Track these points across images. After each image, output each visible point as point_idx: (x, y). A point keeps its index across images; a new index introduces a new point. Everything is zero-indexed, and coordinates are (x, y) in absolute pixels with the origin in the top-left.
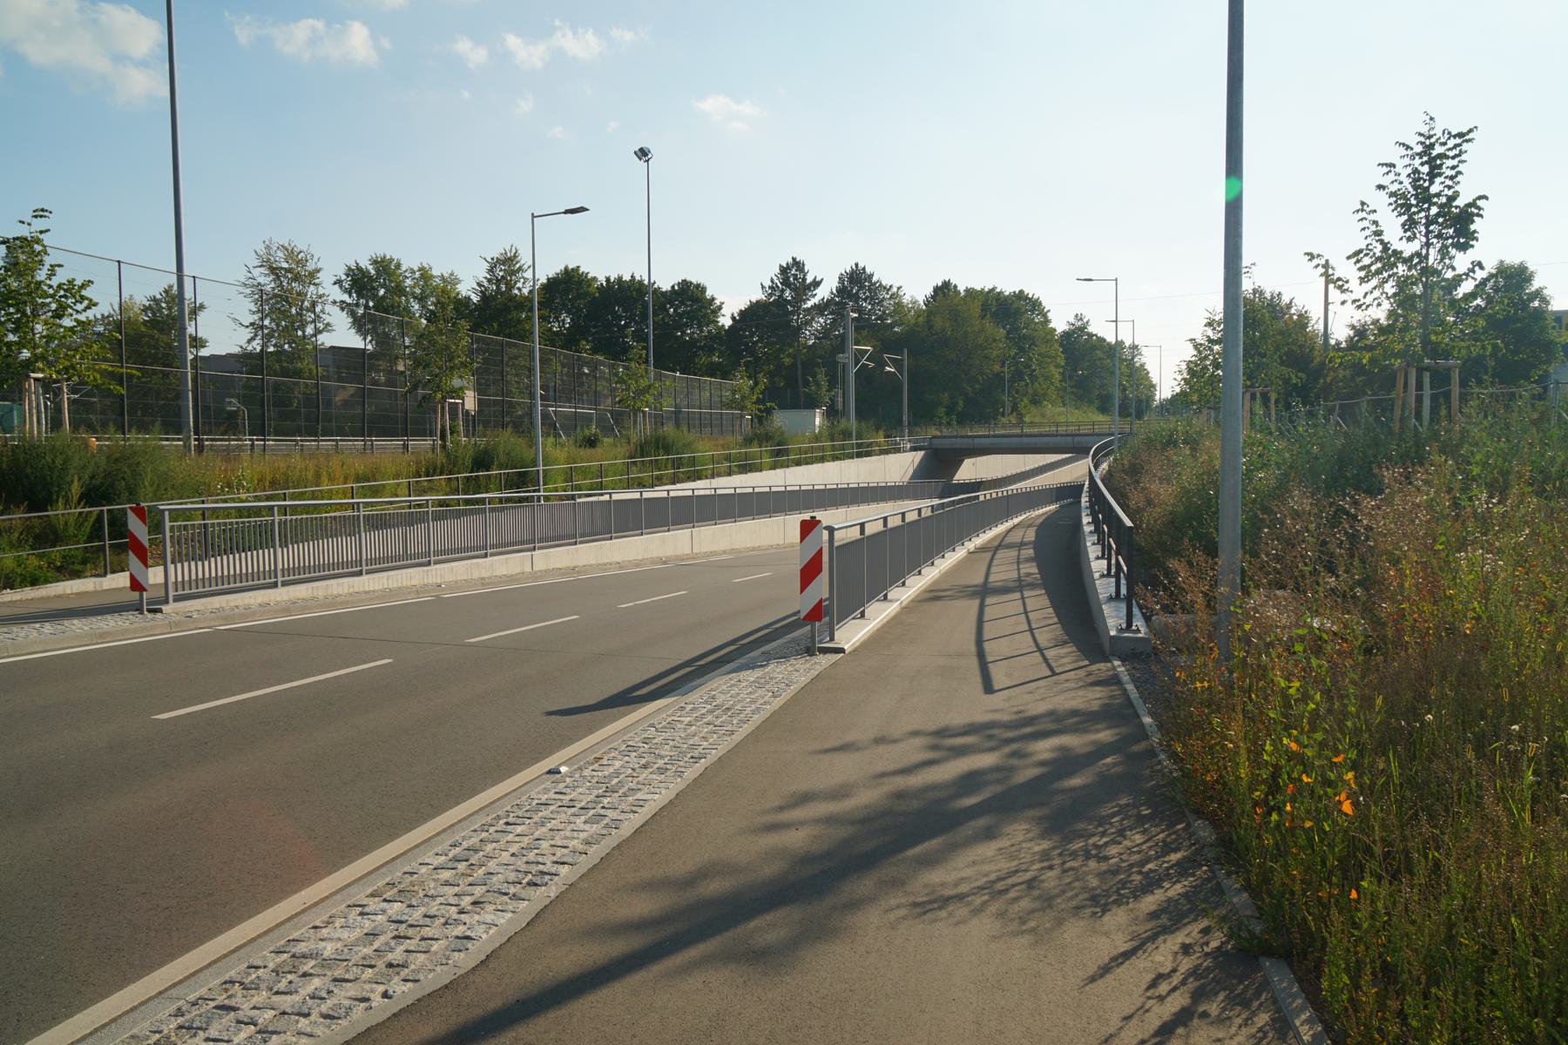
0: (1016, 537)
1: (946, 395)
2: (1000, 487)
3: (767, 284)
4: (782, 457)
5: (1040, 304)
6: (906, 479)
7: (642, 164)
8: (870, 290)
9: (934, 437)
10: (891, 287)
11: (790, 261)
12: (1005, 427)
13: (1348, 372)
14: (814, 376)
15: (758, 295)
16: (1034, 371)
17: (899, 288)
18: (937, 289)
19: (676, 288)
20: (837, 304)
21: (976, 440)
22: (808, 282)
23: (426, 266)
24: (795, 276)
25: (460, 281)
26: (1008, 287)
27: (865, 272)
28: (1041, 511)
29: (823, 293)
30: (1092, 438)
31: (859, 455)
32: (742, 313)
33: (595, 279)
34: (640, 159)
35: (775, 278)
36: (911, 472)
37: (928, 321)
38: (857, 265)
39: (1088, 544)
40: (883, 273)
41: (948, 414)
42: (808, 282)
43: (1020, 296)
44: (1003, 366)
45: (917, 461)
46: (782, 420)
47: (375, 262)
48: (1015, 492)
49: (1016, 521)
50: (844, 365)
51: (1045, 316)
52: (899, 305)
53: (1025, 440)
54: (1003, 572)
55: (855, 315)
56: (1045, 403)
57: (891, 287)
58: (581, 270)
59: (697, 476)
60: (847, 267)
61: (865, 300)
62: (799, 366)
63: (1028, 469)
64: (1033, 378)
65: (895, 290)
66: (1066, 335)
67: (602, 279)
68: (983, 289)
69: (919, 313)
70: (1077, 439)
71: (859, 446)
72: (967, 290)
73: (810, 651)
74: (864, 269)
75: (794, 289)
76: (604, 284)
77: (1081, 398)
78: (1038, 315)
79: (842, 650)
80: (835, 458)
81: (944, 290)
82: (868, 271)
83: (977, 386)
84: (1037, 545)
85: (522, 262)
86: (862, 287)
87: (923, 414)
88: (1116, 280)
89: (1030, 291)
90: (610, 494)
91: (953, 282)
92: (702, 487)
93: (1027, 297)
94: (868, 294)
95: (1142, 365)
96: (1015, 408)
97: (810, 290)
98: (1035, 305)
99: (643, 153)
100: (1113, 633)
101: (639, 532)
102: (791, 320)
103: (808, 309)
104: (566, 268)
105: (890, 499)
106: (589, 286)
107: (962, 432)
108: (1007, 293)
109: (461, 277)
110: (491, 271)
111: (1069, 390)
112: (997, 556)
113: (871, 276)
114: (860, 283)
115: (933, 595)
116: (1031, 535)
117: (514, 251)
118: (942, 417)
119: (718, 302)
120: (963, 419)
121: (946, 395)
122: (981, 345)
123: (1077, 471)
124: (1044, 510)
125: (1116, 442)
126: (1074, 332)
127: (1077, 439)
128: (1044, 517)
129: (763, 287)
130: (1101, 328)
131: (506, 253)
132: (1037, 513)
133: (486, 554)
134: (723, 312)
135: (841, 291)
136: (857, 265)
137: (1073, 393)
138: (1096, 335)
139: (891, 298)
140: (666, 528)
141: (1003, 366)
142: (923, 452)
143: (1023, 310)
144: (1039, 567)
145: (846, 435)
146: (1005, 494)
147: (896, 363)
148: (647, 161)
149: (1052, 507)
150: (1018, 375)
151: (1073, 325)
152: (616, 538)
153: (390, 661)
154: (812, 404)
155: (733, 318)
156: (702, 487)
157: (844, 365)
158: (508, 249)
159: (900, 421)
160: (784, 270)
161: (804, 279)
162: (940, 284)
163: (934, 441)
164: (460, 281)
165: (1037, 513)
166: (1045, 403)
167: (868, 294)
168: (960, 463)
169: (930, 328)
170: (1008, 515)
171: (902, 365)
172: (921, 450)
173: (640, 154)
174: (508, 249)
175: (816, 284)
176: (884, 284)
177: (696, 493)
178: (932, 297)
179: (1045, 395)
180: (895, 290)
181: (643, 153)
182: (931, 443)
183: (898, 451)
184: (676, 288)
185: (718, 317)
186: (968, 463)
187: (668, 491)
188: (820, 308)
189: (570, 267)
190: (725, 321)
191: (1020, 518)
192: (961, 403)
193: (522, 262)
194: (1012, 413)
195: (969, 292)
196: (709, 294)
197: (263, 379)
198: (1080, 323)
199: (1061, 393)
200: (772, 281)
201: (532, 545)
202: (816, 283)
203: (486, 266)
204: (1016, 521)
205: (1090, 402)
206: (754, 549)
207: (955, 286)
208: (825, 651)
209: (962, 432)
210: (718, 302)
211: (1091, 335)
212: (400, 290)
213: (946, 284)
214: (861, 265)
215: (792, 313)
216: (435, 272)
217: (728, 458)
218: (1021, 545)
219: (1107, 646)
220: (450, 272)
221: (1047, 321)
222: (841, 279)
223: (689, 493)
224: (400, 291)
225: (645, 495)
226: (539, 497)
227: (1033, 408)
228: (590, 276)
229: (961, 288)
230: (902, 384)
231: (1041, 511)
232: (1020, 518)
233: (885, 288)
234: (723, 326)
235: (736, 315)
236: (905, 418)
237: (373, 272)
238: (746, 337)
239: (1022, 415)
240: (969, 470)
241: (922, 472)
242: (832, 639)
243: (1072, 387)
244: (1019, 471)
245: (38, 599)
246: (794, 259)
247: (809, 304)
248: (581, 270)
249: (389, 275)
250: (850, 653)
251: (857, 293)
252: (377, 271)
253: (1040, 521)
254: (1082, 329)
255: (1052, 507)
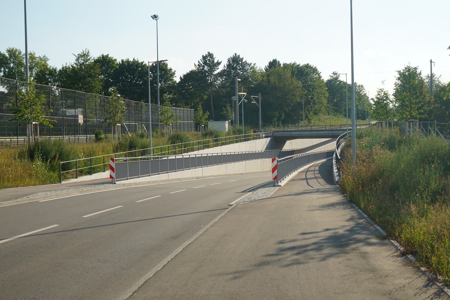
0: (313, 169)
1: (277, 112)
2: (302, 153)
3: (197, 64)
4: (217, 142)
5: (317, 70)
6: (264, 150)
7: (154, 21)
8: (242, 65)
9: (274, 132)
10: (251, 64)
11: (207, 53)
12: (303, 125)
13: (439, 105)
14: (225, 107)
15: (193, 68)
16: (315, 100)
17: (254, 64)
18: (270, 63)
19: (154, 65)
20: (228, 71)
21: (292, 133)
22: (215, 62)
23: (32, 52)
24: (209, 60)
25: (48, 60)
26: (301, 62)
27: (239, 58)
28: (320, 161)
29: (221, 68)
30: (341, 132)
31: (245, 140)
32: (185, 76)
33: (115, 60)
34: (153, 19)
35: (200, 61)
36: (265, 147)
37: (268, 79)
38: (236, 54)
39: (334, 166)
40: (247, 58)
41: (278, 121)
42: (215, 62)
43: (307, 66)
44: (301, 99)
45: (268, 142)
46: (213, 125)
47: (8, 51)
48: (309, 154)
49: (311, 164)
50: (235, 101)
51: (319, 74)
52: (254, 72)
53: (313, 132)
54: (310, 175)
55: (240, 80)
56: (320, 114)
57: (251, 64)
58: (109, 56)
59: (193, 150)
60: (231, 55)
61: (240, 70)
62: (212, 100)
63: (314, 144)
64: (314, 103)
65: (252, 65)
66: (329, 82)
67: (119, 61)
68: (291, 64)
69: (263, 75)
70: (334, 132)
71: (245, 136)
72: (284, 64)
73: (274, 186)
74: (239, 56)
75: (209, 65)
76: (121, 63)
77: (336, 111)
78: (315, 74)
79: (281, 186)
80: (237, 142)
81: (273, 64)
82: (241, 57)
83: (290, 108)
84: (319, 170)
85: (91, 56)
86: (238, 64)
87: (267, 122)
88: (346, 74)
89: (313, 64)
90: (167, 157)
91: (278, 60)
92: (192, 154)
93: (310, 67)
94: (241, 67)
95: (365, 94)
96: (307, 117)
97: (216, 66)
98: (315, 70)
99: (155, 17)
100: (337, 180)
101: (189, 168)
102: (208, 80)
103: (215, 75)
104: (103, 55)
105: (254, 159)
106: (114, 63)
107: (286, 129)
108: (301, 65)
109: (49, 58)
110: (77, 60)
111: (331, 107)
112: (307, 173)
113: (242, 59)
114: (237, 62)
115: (292, 180)
116: (317, 168)
117: (87, 51)
118: (275, 122)
119: (173, 71)
120: (285, 123)
121: (277, 112)
122: (291, 90)
123: (332, 146)
124: (321, 161)
125: (347, 134)
126: (332, 80)
127: (334, 132)
128: (321, 163)
129: (195, 65)
130: (346, 78)
131: (84, 52)
132: (319, 162)
133: (128, 178)
134: (175, 75)
135: (229, 66)
136: (236, 54)
137: (333, 109)
138: (342, 82)
139: (251, 69)
140: (207, 166)
141: (301, 99)
142: (269, 139)
143: (309, 73)
144: (320, 175)
145: (240, 132)
146: (304, 155)
147: (257, 100)
148: (157, 20)
149: (324, 160)
150: (308, 102)
151: (332, 77)
152: (130, 179)
153: (58, 225)
154: (224, 118)
155: (181, 78)
156: (192, 154)
157: (235, 101)
158: (84, 50)
159: (258, 124)
160: (204, 58)
161: (213, 61)
162: (272, 61)
163: (275, 133)
164: (48, 60)
165: (319, 162)
166: (320, 114)
167: (241, 67)
168: (284, 143)
169: (269, 82)
170: (309, 162)
171: (259, 101)
172: (269, 137)
173: (153, 17)
174: (84, 50)
175: (219, 63)
176: (248, 62)
177: (191, 156)
178: (268, 67)
179: (320, 110)
180: (252, 65)
181: (155, 17)
182: (273, 134)
183: (260, 138)
184: (154, 65)
185: (173, 77)
186: (288, 142)
187: (183, 156)
188: (220, 74)
189: (105, 55)
190: (177, 79)
191: (313, 164)
192: (283, 116)
193: (91, 56)
194: (305, 119)
195: (285, 66)
196: (169, 67)
197: (63, 118)
198: (335, 76)
199: (327, 109)
200: (199, 62)
201: (149, 174)
202: (219, 63)
203: (75, 58)
204: (311, 164)
205: (341, 113)
206: (219, 175)
207: (279, 62)
208: (277, 186)
209: (286, 129)
210: (173, 71)
211: (340, 82)
212: (20, 64)
213: (275, 61)
214: (238, 54)
215: (207, 76)
216: (37, 55)
217: (199, 143)
218: (314, 171)
219: (335, 183)
220: (43, 55)
221: (320, 77)
222: (229, 61)
223: (188, 156)
224: (21, 65)
225: (177, 157)
226: (151, 158)
227: (315, 116)
228: (113, 59)
229: (282, 63)
230: (258, 108)
231: (320, 161)
232: (313, 164)
233: (248, 64)
234: (176, 81)
235: (182, 77)
236: (260, 123)
237: (7, 56)
238: (186, 86)
239: (309, 119)
240: (289, 146)
241: (270, 147)
242: (278, 184)
243: (332, 106)
244: (310, 146)
245: (72, 183)
246: (209, 53)
247: (216, 73)
248: (109, 56)
249: (15, 57)
250: (283, 186)
251: (236, 67)
252: (10, 55)
253: (320, 164)
254: (336, 79)
255: (324, 160)
